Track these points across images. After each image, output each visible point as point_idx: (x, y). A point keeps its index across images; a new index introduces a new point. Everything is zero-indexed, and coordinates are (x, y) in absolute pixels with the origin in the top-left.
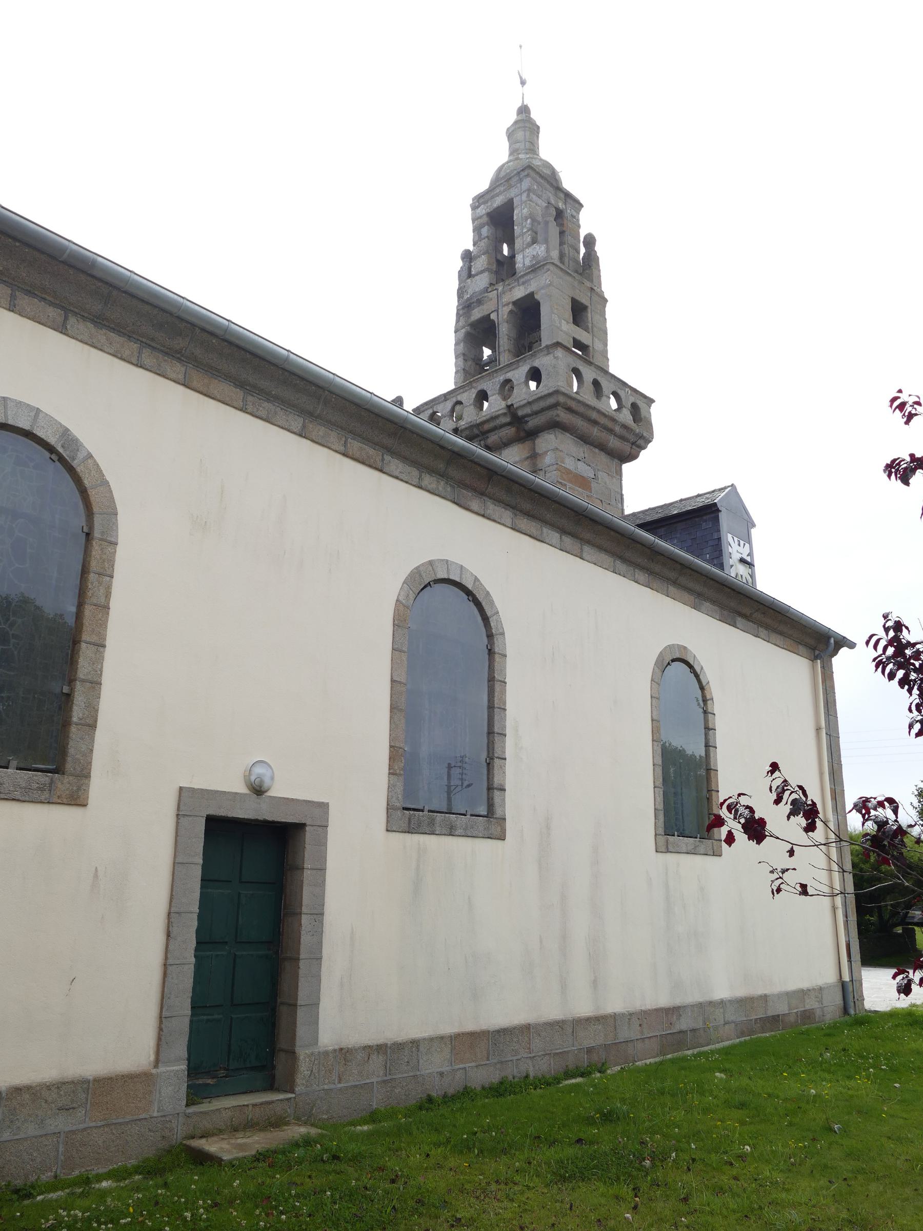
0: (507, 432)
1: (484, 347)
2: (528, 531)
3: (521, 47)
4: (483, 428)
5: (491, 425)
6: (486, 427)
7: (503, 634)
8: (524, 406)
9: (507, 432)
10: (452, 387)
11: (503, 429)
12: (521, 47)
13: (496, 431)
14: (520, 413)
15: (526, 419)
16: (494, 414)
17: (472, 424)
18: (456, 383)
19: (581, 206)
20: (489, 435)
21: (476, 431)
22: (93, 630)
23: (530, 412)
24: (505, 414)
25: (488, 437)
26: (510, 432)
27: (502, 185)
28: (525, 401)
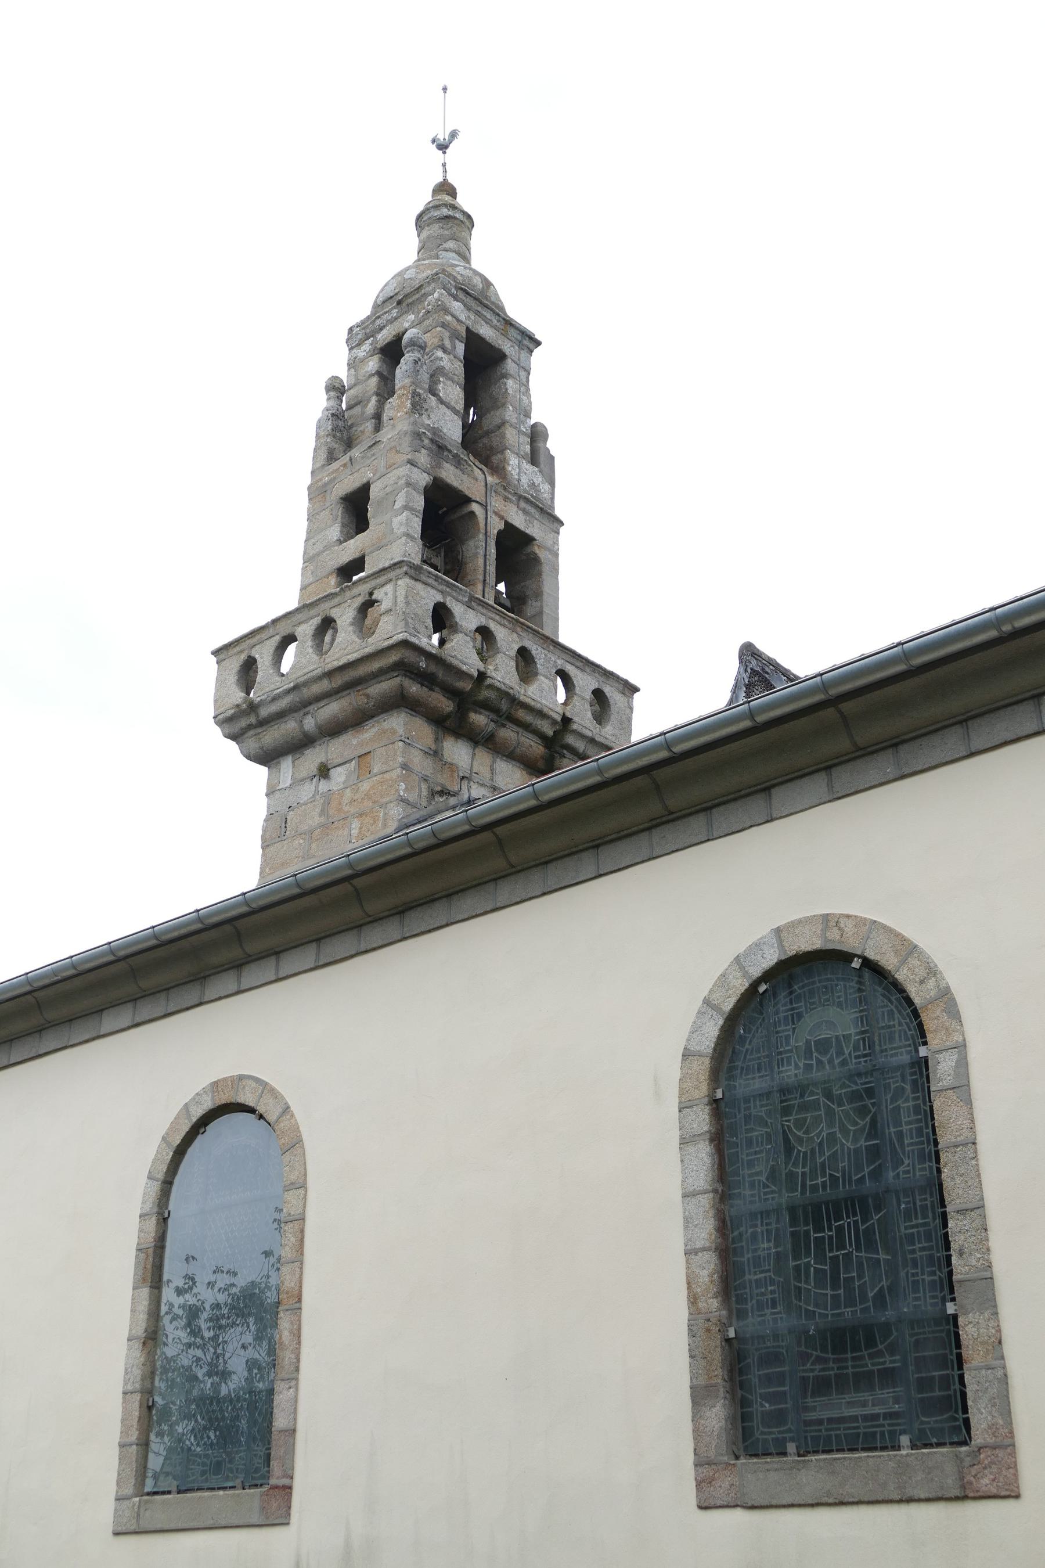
0: (532, 743)
1: (503, 583)
2: (948, 1043)
3: (445, 89)
4: (517, 710)
5: (529, 718)
6: (521, 714)
7: (687, 1055)
8: (583, 736)
9: (532, 743)
10: (293, 604)
11: (530, 736)
12: (445, 89)
13: (520, 730)
14: (570, 740)
15: (565, 752)
16: (545, 710)
17: (511, 691)
18: (299, 603)
19: (562, 523)
20: (509, 725)
21: (504, 705)
22: (748, 1118)
23: (581, 750)
24: (554, 722)
25: (504, 726)
26: (535, 748)
27: (497, 317)
28: (589, 734)
